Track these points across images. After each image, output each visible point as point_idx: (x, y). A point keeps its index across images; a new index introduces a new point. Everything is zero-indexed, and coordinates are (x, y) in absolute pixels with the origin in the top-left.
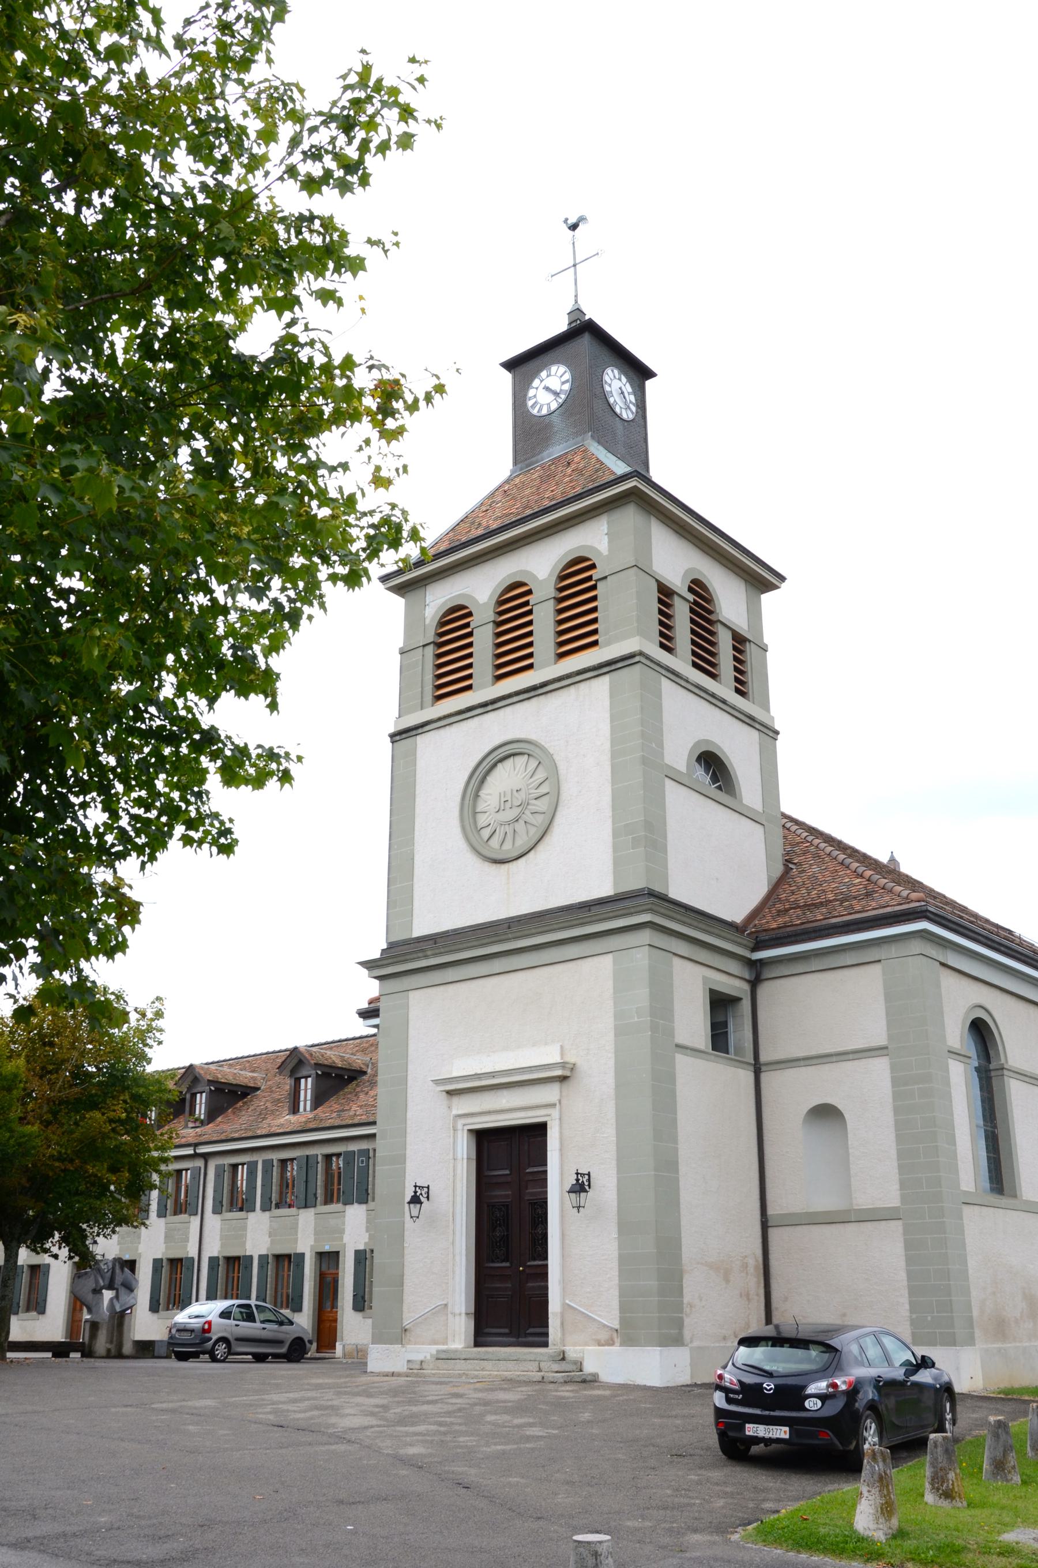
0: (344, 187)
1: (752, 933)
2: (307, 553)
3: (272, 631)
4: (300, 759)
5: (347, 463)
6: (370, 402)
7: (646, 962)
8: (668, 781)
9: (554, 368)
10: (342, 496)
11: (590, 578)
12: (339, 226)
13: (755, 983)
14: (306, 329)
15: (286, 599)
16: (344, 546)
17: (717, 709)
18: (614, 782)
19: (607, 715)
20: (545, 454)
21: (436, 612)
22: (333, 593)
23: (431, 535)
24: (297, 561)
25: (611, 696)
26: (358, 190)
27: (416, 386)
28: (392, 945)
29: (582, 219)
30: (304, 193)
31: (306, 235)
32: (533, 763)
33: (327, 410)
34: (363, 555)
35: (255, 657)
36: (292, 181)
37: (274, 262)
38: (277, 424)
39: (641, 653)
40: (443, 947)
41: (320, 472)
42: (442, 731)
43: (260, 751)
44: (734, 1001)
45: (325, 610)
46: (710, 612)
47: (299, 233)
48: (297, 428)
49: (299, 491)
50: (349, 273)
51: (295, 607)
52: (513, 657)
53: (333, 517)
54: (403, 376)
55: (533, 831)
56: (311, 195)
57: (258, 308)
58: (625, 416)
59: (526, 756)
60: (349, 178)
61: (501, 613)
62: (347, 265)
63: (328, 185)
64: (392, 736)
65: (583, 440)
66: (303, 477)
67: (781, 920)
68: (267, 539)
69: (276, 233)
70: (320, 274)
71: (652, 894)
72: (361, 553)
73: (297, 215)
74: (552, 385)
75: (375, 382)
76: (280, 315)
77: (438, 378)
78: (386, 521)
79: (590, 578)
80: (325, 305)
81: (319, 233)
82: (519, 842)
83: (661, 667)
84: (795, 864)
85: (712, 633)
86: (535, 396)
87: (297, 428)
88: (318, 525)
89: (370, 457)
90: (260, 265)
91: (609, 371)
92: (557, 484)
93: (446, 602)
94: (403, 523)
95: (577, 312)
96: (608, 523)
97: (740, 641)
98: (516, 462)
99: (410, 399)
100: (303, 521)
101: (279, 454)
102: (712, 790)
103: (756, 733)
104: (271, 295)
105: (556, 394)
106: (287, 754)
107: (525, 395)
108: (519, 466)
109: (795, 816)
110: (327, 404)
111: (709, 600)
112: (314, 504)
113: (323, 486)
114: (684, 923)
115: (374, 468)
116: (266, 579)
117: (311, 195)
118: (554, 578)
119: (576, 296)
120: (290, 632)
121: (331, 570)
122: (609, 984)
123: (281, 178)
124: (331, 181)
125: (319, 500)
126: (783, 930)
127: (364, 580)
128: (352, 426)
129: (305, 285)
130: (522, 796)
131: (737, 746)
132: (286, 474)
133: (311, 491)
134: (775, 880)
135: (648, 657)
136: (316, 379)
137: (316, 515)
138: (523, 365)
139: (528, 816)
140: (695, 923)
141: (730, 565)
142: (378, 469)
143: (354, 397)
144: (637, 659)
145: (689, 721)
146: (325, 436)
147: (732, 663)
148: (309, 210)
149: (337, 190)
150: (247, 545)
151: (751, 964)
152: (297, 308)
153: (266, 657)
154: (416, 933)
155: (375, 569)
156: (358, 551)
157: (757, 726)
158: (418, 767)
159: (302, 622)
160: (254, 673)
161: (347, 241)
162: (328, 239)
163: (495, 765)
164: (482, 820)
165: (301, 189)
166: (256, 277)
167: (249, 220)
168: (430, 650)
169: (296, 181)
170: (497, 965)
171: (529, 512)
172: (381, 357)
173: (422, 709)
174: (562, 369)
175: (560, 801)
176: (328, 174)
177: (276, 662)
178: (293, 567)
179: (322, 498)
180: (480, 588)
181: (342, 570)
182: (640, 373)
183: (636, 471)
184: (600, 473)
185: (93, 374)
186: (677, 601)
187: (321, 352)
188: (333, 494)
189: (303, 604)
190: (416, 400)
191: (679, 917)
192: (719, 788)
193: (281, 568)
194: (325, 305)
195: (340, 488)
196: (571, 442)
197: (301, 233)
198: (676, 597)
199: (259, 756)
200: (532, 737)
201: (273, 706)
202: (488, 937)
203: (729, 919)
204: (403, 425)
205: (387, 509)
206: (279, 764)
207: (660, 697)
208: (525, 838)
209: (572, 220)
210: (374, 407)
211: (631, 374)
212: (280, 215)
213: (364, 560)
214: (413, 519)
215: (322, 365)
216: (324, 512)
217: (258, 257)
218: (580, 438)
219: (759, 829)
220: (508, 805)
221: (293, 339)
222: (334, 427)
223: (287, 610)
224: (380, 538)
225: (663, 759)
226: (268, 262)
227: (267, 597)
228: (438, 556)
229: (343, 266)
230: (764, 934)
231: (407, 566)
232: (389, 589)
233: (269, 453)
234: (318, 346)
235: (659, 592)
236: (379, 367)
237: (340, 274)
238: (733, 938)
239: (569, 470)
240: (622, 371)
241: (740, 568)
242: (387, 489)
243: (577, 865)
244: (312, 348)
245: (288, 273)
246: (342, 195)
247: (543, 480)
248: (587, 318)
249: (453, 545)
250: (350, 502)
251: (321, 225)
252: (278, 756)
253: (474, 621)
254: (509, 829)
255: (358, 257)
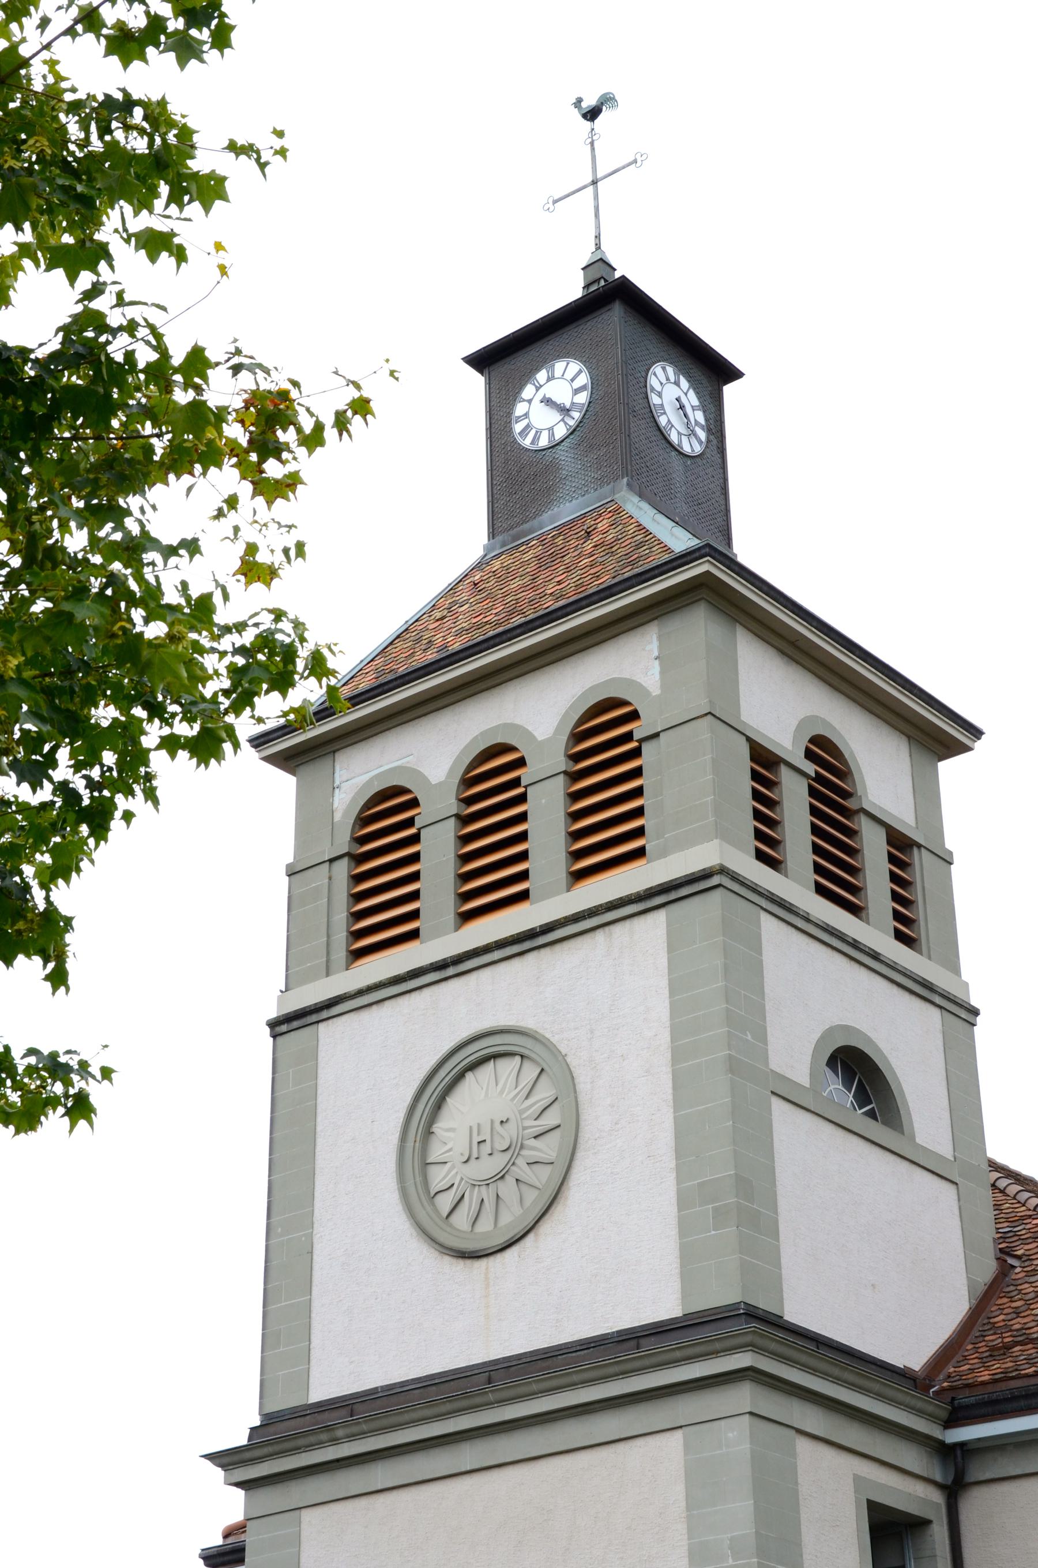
0: (186, 50)
1: (943, 1390)
2: (123, 700)
3: (58, 839)
4: (107, 1073)
5: (195, 541)
6: (235, 432)
7: (746, 1447)
8: (777, 1104)
9: (559, 366)
10: (188, 599)
11: (628, 737)
12: (178, 118)
13: (954, 1490)
14: (120, 301)
15: (84, 782)
16: (191, 689)
17: (863, 970)
18: (678, 1104)
19: (663, 983)
20: (545, 516)
21: (354, 800)
22: (171, 771)
23: (342, 664)
24: (105, 714)
25: (671, 948)
26: (212, 55)
27: (319, 402)
28: (270, 1420)
29: (607, 100)
30: (114, 59)
31: (119, 135)
32: (530, 1072)
33: (159, 446)
34: (225, 703)
35: (26, 888)
36: (91, 36)
37: (60, 181)
38: (69, 472)
39: (723, 870)
40: (368, 1420)
41: (149, 556)
42: (364, 1014)
43: (32, 1060)
44: (918, 1525)
45: (156, 802)
46: (846, 795)
47: (105, 130)
48: (104, 478)
49: (109, 592)
50: (196, 205)
51: (101, 797)
52: (492, 876)
53: (173, 638)
54: (295, 384)
55: (530, 1196)
56: (126, 64)
57: (27, 263)
58: (686, 448)
59: (518, 1059)
60: (194, 32)
61: (469, 801)
62: (194, 188)
63: (157, 45)
64: (273, 1024)
65: (613, 492)
66: (117, 566)
67: (997, 1367)
68: (51, 675)
69: (63, 129)
70: (144, 204)
71: (752, 1314)
72: (221, 699)
73: (101, 98)
74: (556, 396)
75: (246, 396)
76: (72, 278)
77: (358, 387)
78: (265, 641)
79: (628, 737)
80: (153, 258)
81: (142, 132)
82: (505, 1219)
83: (760, 894)
84: (1018, 1257)
85: (851, 833)
86: (526, 415)
87: (104, 478)
88: (146, 653)
89: (236, 529)
90: (34, 187)
91: (657, 369)
92: (568, 570)
93: (371, 780)
94: (297, 644)
95: (600, 264)
96: (660, 638)
97: (901, 846)
98: (493, 531)
99: (307, 425)
100: (117, 646)
101: (73, 524)
102: (858, 1119)
103: (936, 1013)
104: (52, 242)
105: (564, 411)
106: (84, 1065)
107: (510, 414)
108: (499, 538)
109: (1014, 1166)
110: (159, 436)
111: (844, 773)
112: (137, 615)
113: (152, 581)
114: (814, 1371)
115: (244, 546)
116: (47, 748)
117: (126, 64)
118: (564, 738)
119: (598, 237)
120: (91, 842)
121: (166, 731)
122: (678, 1492)
123: (71, 32)
124: (163, 38)
125: (146, 608)
126: (1003, 1386)
127: (227, 747)
128: (204, 474)
129: (117, 223)
130: (507, 1135)
131: (902, 1037)
132: (86, 560)
133: (133, 593)
134: (981, 1289)
135: (735, 877)
136: (138, 389)
137: (142, 633)
138: (504, 361)
139: (522, 1170)
140: (836, 1372)
141: (879, 710)
142: (252, 549)
143: (209, 423)
144: (715, 880)
145: (814, 992)
146: (156, 493)
147: (887, 885)
148: (124, 91)
149: (172, 55)
150: (14, 690)
151: (946, 1452)
152: (103, 266)
153: (45, 886)
154: (317, 1394)
155: (245, 726)
156: (215, 694)
157: (938, 1000)
158: (321, 1081)
159: (113, 824)
160: (25, 918)
161: (193, 147)
162: (158, 141)
163: (460, 1076)
164: (438, 1178)
165: (109, 52)
166: (28, 208)
167: (12, 105)
168: (342, 869)
169: (98, 36)
170: (468, 1455)
171: (517, 620)
172: (254, 349)
173: (328, 975)
174: (574, 366)
175: (581, 1140)
176: (156, 24)
177: (65, 897)
178: (98, 725)
179: (152, 605)
180: (432, 756)
181: (184, 730)
182: (712, 371)
183: (708, 545)
184: (644, 551)
185: (294, 641)
186: (785, 775)
187: (148, 343)
188: (171, 597)
189: (115, 791)
190: (319, 427)
191: (804, 1358)
192: (872, 1114)
193: (73, 726)
194: (153, 258)
195: (184, 585)
196: (592, 495)
197: (110, 132)
198: (784, 770)
199: (30, 1070)
200: (528, 1023)
201: (58, 978)
202: (449, 1399)
203: (898, 1362)
204: (297, 473)
205: (266, 621)
206: (68, 1083)
207: (759, 951)
208: (518, 1211)
209: (590, 102)
210: (244, 441)
211: (697, 373)
212: (68, 97)
213: (226, 712)
214: (315, 638)
215: (149, 365)
216: (156, 630)
217: (30, 171)
218: (607, 489)
219: (948, 1192)
220: (486, 1148)
221: (97, 321)
222: (172, 477)
223: (86, 802)
224: (256, 672)
225: (767, 1064)
226: (50, 181)
227: (50, 779)
228: (357, 700)
229: (186, 191)
230: (967, 1392)
231: (299, 720)
232: (266, 759)
233: (55, 523)
234: (143, 332)
235: (752, 759)
236: (255, 367)
237: (181, 206)
238: (908, 1400)
239: (589, 546)
240: (681, 370)
241: (898, 715)
242: (268, 585)
243: (614, 1261)
244: (133, 336)
245: (86, 202)
246: (182, 63)
247: (543, 563)
248: (617, 275)
249: (382, 680)
250: (203, 608)
251: (146, 118)
252: (67, 1068)
253: (423, 815)
254: (487, 1194)
255: (212, 175)
